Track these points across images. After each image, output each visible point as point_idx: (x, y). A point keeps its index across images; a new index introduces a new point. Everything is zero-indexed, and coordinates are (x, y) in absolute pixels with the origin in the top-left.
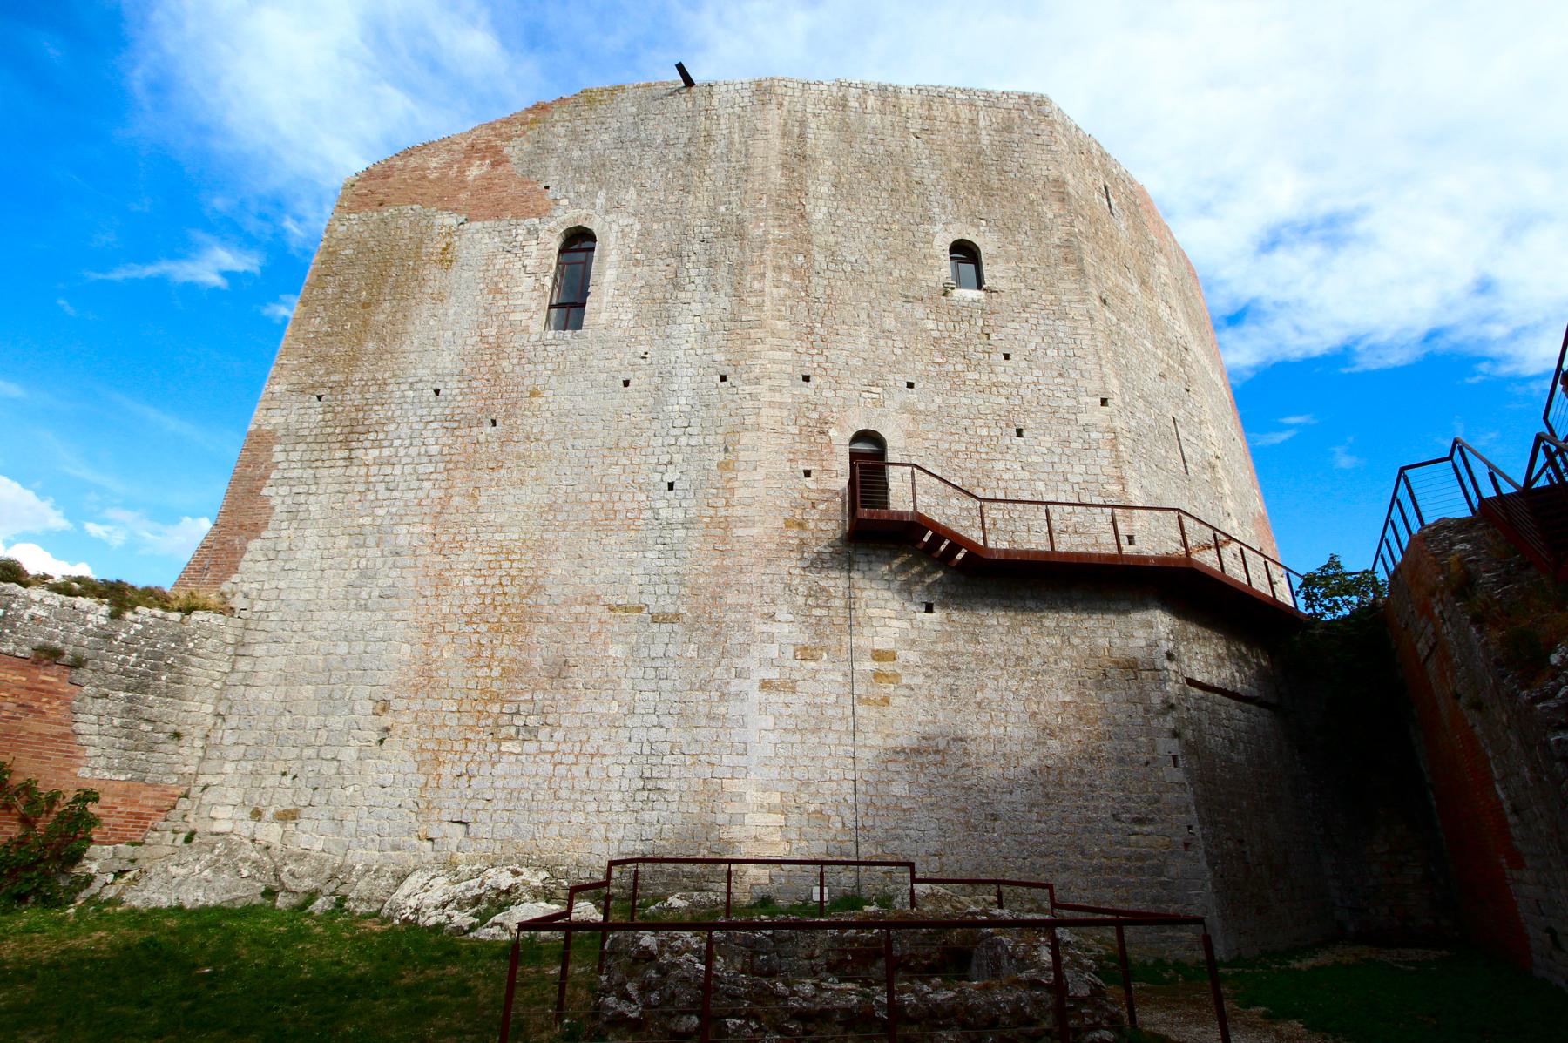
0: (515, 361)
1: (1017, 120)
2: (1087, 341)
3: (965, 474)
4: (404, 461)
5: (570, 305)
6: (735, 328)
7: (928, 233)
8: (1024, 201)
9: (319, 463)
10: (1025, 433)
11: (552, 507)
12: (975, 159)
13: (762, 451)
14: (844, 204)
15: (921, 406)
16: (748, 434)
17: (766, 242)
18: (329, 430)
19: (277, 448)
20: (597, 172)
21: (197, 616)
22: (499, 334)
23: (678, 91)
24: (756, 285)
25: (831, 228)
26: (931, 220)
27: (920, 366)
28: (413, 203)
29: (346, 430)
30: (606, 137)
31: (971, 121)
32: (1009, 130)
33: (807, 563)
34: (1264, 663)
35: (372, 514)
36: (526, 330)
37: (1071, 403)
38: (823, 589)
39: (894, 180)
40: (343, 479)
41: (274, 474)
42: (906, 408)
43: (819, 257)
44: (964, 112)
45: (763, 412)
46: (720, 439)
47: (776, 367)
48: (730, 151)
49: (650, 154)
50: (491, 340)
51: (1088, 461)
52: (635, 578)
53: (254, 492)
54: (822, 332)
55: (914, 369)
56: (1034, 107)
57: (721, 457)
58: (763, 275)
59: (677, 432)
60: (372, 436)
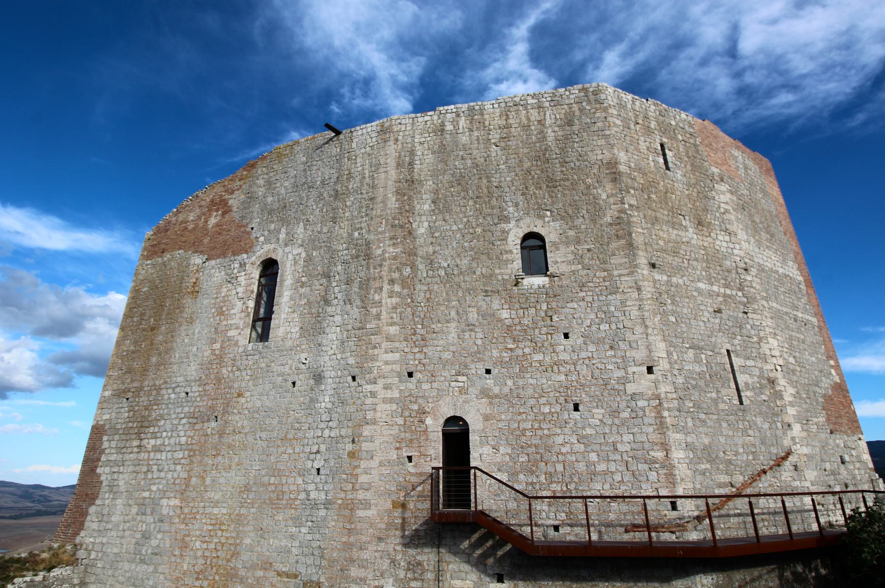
0: (230, 369)
1: (577, 113)
2: (635, 313)
3: (532, 450)
4: (168, 448)
5: (262, 323)
6: (361, 336)
7: (503, 232)
8: (582, 187)
9: (124, 450)
10: (581, 408)
11: (247, 488)
12: (542, 157)
13: (377, 442)
14: (440, 217)
15: (496, 390)
16: (368, 427)
17: (384, 260)
18: (131, 424)
19: (105, 438)
20: (281, 213)
21: (56, 572)
22: (222, 347)
23: (331, 139)
24: (377, 297)
25: (431, 240)
26: (507, 219)
27: (495, 353)
28: (179, 249)
29: (139, 425)
30: (286, 184)
31: (539, 122)
32: (570, 123)
33: (408, 540)
34: (823, 572)
35: (150, 490)
36: (236, 344)
37: (620, 373)
38: (419, 564)
39: (479, 187)
40: (136, 462)
41: (103, 458)
42: (485, 393)
43: (421, 267)
44: (534, 115)
45: (379, 408)
46: (350, 431)
47: (389, 368)
48: (362, 185)
49: (314, 193)
50: (217, 352)
51: (635, 430)
52: (294, 550)
53: (93, 470)
54: (423, 332)
55: (491, 357)
56: (592, 97)
57: (349, 447)
58: (381, 289)
59: (323, 425)
60: (151, 430)
